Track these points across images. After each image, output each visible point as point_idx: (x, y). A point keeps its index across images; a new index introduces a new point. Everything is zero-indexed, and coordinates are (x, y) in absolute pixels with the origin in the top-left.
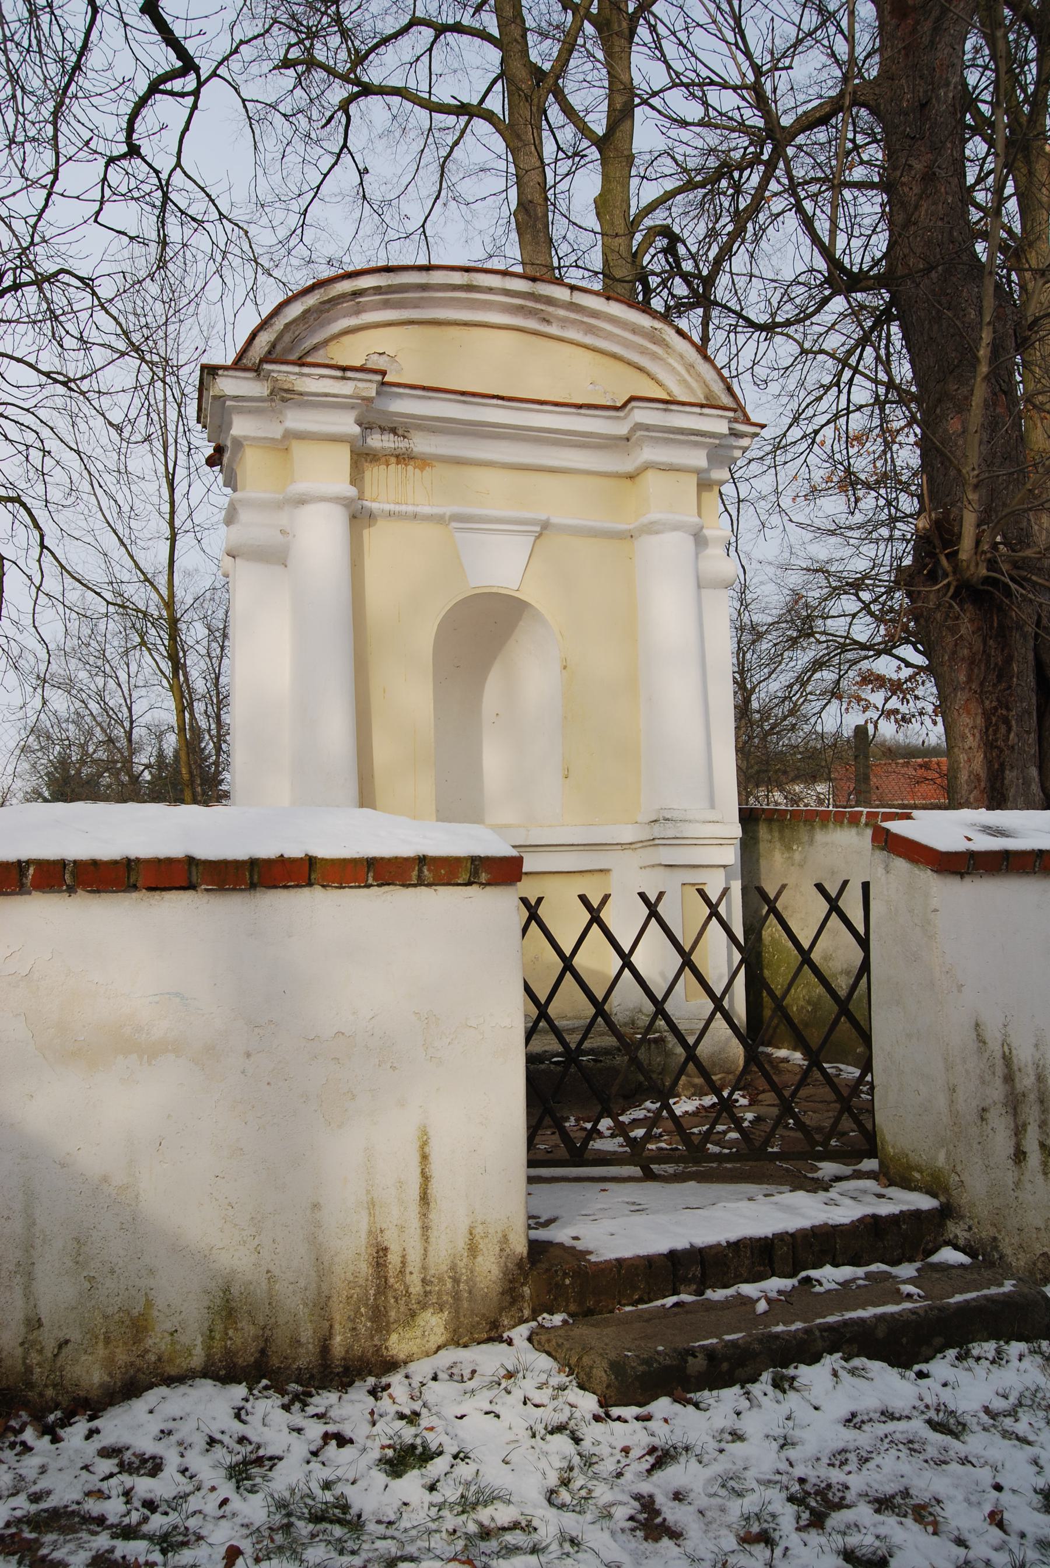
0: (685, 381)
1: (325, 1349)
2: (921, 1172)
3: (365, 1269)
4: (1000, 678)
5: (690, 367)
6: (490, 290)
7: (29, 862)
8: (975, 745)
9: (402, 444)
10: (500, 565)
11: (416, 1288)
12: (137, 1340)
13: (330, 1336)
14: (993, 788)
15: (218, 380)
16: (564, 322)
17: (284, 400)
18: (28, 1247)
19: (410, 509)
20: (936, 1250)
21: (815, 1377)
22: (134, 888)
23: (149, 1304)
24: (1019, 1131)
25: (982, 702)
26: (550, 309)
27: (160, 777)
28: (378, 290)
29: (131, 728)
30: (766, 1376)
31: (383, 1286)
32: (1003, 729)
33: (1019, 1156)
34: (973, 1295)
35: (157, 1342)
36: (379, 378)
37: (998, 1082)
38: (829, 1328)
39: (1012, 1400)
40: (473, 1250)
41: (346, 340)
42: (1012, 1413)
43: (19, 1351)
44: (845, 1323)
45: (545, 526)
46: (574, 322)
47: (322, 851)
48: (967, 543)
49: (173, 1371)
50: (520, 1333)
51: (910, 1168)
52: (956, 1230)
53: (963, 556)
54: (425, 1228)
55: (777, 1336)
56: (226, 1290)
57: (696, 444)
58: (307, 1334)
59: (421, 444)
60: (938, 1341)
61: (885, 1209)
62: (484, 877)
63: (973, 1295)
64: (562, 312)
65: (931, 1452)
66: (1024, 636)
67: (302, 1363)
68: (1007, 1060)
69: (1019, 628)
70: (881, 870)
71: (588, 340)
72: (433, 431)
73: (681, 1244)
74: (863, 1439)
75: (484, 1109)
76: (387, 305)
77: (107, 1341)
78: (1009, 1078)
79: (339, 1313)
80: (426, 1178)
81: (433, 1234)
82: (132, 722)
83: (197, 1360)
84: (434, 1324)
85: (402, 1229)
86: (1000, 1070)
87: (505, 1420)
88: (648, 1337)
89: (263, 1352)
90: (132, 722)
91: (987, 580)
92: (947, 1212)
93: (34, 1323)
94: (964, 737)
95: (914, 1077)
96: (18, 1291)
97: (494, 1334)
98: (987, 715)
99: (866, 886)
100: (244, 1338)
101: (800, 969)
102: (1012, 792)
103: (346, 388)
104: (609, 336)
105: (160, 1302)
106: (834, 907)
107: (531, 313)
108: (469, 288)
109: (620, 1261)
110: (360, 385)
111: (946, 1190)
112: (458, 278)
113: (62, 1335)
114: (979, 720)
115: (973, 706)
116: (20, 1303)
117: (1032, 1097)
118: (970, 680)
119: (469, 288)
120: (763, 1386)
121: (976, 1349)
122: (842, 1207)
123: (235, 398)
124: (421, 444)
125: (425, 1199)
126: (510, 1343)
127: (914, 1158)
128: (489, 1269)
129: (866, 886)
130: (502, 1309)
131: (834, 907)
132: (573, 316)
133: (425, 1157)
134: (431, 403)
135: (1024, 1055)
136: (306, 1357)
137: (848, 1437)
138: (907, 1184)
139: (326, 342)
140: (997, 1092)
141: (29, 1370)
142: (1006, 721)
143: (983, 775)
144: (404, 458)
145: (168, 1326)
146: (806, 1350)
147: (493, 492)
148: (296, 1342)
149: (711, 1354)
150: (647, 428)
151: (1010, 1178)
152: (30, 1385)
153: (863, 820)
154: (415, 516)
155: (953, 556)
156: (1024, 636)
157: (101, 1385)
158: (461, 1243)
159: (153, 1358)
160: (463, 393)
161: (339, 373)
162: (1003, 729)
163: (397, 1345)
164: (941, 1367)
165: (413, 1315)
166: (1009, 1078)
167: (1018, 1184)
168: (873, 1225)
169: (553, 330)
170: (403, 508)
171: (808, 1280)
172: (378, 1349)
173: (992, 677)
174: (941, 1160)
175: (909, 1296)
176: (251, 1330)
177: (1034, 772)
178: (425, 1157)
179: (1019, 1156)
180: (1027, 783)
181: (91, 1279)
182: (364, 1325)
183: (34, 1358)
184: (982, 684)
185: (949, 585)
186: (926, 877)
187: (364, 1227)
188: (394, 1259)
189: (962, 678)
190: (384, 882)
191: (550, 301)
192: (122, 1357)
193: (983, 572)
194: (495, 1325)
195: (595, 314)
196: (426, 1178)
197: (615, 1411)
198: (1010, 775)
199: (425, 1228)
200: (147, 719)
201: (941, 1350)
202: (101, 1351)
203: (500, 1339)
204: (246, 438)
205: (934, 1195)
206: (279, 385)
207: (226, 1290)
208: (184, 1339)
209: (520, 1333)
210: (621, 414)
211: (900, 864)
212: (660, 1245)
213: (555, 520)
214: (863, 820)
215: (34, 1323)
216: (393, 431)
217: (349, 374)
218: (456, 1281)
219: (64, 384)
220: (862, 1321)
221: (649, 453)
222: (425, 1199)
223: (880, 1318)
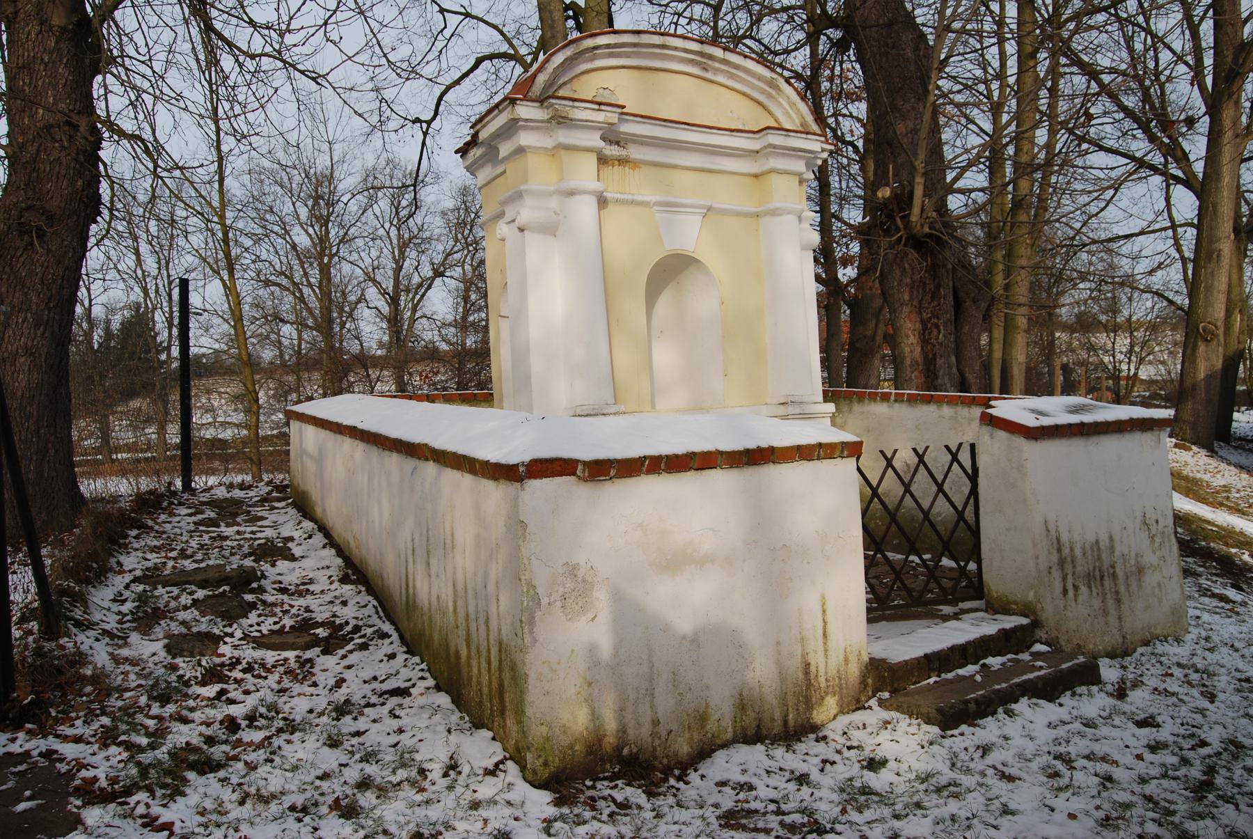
0: (788, 113)
1: (785, 722)
2: (1016, 604)
3: (801, 675)
4: (933, 298)
5: (792, 105)
6: (676, 49)
7: (645, 457)
8: (915, 341)
9: (623, 153)
10: (689, 235)
11: (823, 685)
12: (703, 727)
13: (786, 716)
14: (928, 370)
15: (517, 107)
16: (717, 70)
17: (559, 123)
18: (651, 680)
19: (630, 197)
20: (1031, 646)
21: (1022, 706)
22: (690, 469)
23: (707, 706)
24: (1064, 579)
25: (921, 313)
26: (710, 62)
27: (108, 348)
28: (608, 46)
29: (90, 305)
30: (1000, 710)
31: (809, 685)
32: (935, 331)
33: (1065, 592)
34: (1069, 664)
35: (711, 726)
36: (620, 110)
37: (1055, 552)
38: (1018, 685)
39: (1108, 711)
40: (846, 660)
41: (584, 78)
42: (1110, 717)
43: (650, 739)
44: (1025, 681)
45: (709, 209)
46: (723, 71)
47: (776, 444)
48: (916, 210)
49: (719, 742)
50: (873, 702)
51: (1009, 603)
52: (1040, 634)
53: (914, 219)
54: (826, 651)
55: (999, 690)
56: (741, 694)
57: (800, 157)
58: (777, 715)
59: (635, 152)
60: (1061, 688)
61: (1008, 626)
62: (846, 453)
63: (1069, 664)
64: (717, 65)
65: (1090, 737)
66: (947, 271)
67: (775, 731)
68: (1058, 539)
69: (944, 266)
70: (987, 437)
71: (730, 83)
72: (642, 144)
73: (929, 651)
74: (1062, 731)
75: (844, 583)
76: (611, 55)
77: (689, 728)
78: (1059, 550)
79: (791, 701)
80: (825, 623)
81: (829, 653)
82: (90, 301)
83: (729, 735)
84: (832, 703)
85: (815, 652)
86: (1055, 545)
87: (905, 744)
88: (952, 696)
89: (758, 727)
90: (90, 301)
91: (929, 236)
92: (1036, 624)
93: (656, 722)
94: (908, 337)
95: (1008, 554)
96: (648, 705)
97: (860, 707)
98: (924, 323)
99: (973, 446)
100: (750, 719)
101: (936, 496)
102: (941, 373)
103: (600, 117)
104: (743, 81)
105: (712, 704)
106: (955, 458)
107: (697, 64)
108: (663, 47)
109: (906, 662)
110: (609, 115)
111: (1034, 612)
112: (657, 40)
113: (668, 728)
114: (918, 326)
115: (913, 316)
116: (649, 712)
117: (1069, 559)
118: (911, 299)
119: (663, 47)
120: (1000, 714)
121: (1079, 690)
122: (988, 627)
123: (527, 120)
124: (635, 152)
125: (825, 634)
126: (870, 708)
127: (1011, 597)
128: (854, 671)
129: (973, 446)
130: (860, 692)
131: (955, 458)
132: (723, 67)
133: (824, 611)
134: (644, 126)
135: (1065, 537)
136: (777, 728)
137: (1053, 733)
138: (1007, 611)
139: (571, 80)
140: (1054, 558)
141: (655, 749)
142: (937, 327)
143: (920, 361)
144: (623, 161)
145: (716, 717)
146: (1009, 697)
147: (686, 186)
148: (773, 720)
149: (976, 701)
150: (774, 147)
151: (1062, 603)
152: (655, 758)
153: (893, 398)
154: (632, 202)
155: (906, 218)
156: (947, 271)
157: (688, 754)
158: (841, 658)
159: (710, 735)
160: (665, 120)
161: (596, 107)
162: (935, 331)
163: (818, 716)
164: (1066, 699)
165: (822, 698)
166: (1059, 550)
167: (1065, 607)
168: (1004, 633)
169: (709, 76)
170: (626, 197)
171: (984, 665)
172: (808, 719)
173: (928, 297)
174: (1031, 596)
175: (1041, 667)
176: (753, 715)
177: (953, 359)
178: (824, 611)
179: (1065, 592)
180: (950, 367)
181: (680, 694)
182: (802, 707)
183: (657, 742)
184: (920, 302)
185: (901, 238)
186: (1020, 441)
187: (799, 652)
188: (813, 669)
189: (906, 297)
190: (809, 458)
191: (711, 57)
192: (696, 737)
193: (927, 230)
194: (858, 701)
195: (737, 67)
196: (825, 623)
197: (950, 732)
198: (939, 362)
199: (826, 651)
200: (103, 299)
201: (1063, 692)
202: (687, 735)
203: (864, 708)
204: (529, 147)
205: (1026, 616)
206: (559, 113)
207: (741, 694)
208: (723, 723)
209: (873, 702)
210: (756, 136)
211: (1002, 434)
212: (918, 652)
213: (715, 205)
214: (893, 398)
215: (656, 722)
216: (618, 143)
217: (603, 107)
218: (840, 678)
219: (314, 79)
220: (1030, 680)
221: (774, 163)
222: (825, 634)
223: (1038, 677)
